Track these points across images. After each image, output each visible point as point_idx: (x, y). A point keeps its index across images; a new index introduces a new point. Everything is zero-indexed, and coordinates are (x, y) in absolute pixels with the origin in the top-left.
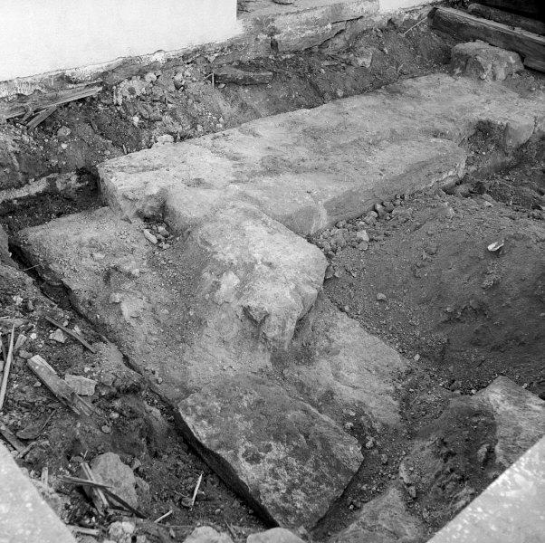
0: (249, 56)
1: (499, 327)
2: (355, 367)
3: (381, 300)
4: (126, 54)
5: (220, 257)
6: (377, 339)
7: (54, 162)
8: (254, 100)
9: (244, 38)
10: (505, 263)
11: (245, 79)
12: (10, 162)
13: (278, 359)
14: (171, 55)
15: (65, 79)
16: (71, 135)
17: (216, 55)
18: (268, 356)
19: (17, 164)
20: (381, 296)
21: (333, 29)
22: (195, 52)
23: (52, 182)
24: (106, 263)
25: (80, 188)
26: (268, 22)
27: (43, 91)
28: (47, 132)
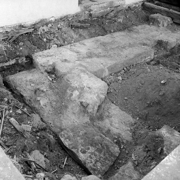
0: (82, 19)
1: (165, 108)
2: (117, 122)
3: (126, 100)
4: (42, 18)
5: (73, 85)
6: (124, 112)
7: (18, 54)
8: (84, 33)
9: (81, 12)
10: (167, 87)
11: (81, 26)
12: (3, 54)
13: (92, 119)
14: (57, 18)
15: (21, 26)
16: (24, 45)
17: (71, 18)
18: (89, 118)
19: (6, 55)
20: (126, 98)
21: (110, 10)
22: (65, 17)
23: (17, 60)
24: (35, 87)
25: (26, 62)
26: (88, 7)
27: (14, 30)
28: (15, 44)
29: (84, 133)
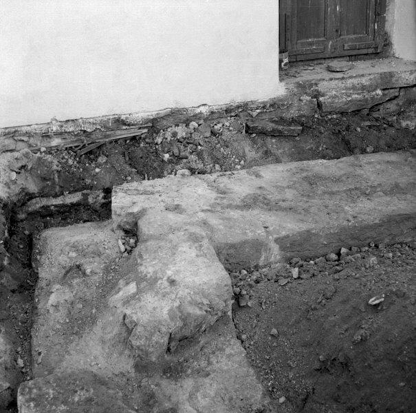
0: (293, 113)
1: (359, 387)
2: (212, 393)
3: (272, 336)
4: (173, 106)
5: (142, 269)
6: (252, 371)
7: (88, 181)
8: (278, 149)
9: (285, 98)
10: (380, 320)
11: (274, 130)
12: (52, 177)
13: (142, 366)
14: (215, 108)
15: (120, 122)
16: (106, 163)
17: (258, 111)
18: (132, 362)
19: (57, 180)
20: (274, 331)
21: (384, 95)
22: (238, 107)
23: (86, 196)
24: (75, 260)
25: (104, 204)
26: (311, 85)
27: (103, 129)
28: (90, 159)
29: (86, 398)
